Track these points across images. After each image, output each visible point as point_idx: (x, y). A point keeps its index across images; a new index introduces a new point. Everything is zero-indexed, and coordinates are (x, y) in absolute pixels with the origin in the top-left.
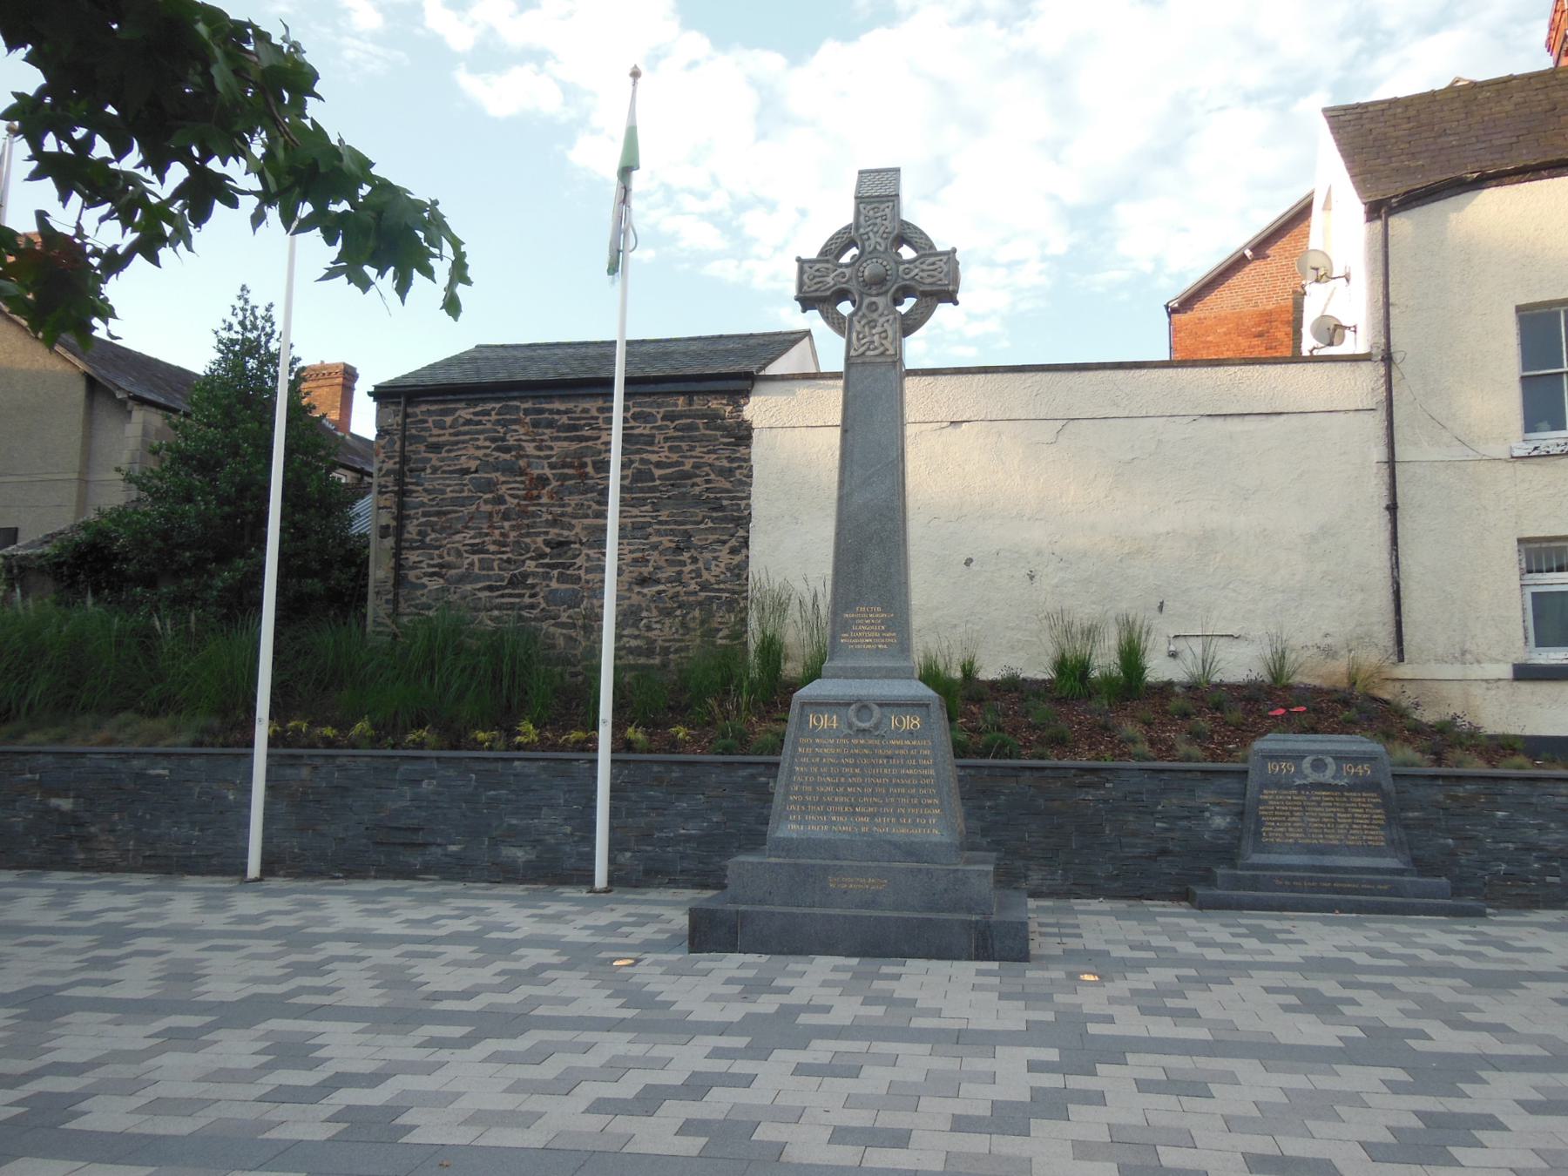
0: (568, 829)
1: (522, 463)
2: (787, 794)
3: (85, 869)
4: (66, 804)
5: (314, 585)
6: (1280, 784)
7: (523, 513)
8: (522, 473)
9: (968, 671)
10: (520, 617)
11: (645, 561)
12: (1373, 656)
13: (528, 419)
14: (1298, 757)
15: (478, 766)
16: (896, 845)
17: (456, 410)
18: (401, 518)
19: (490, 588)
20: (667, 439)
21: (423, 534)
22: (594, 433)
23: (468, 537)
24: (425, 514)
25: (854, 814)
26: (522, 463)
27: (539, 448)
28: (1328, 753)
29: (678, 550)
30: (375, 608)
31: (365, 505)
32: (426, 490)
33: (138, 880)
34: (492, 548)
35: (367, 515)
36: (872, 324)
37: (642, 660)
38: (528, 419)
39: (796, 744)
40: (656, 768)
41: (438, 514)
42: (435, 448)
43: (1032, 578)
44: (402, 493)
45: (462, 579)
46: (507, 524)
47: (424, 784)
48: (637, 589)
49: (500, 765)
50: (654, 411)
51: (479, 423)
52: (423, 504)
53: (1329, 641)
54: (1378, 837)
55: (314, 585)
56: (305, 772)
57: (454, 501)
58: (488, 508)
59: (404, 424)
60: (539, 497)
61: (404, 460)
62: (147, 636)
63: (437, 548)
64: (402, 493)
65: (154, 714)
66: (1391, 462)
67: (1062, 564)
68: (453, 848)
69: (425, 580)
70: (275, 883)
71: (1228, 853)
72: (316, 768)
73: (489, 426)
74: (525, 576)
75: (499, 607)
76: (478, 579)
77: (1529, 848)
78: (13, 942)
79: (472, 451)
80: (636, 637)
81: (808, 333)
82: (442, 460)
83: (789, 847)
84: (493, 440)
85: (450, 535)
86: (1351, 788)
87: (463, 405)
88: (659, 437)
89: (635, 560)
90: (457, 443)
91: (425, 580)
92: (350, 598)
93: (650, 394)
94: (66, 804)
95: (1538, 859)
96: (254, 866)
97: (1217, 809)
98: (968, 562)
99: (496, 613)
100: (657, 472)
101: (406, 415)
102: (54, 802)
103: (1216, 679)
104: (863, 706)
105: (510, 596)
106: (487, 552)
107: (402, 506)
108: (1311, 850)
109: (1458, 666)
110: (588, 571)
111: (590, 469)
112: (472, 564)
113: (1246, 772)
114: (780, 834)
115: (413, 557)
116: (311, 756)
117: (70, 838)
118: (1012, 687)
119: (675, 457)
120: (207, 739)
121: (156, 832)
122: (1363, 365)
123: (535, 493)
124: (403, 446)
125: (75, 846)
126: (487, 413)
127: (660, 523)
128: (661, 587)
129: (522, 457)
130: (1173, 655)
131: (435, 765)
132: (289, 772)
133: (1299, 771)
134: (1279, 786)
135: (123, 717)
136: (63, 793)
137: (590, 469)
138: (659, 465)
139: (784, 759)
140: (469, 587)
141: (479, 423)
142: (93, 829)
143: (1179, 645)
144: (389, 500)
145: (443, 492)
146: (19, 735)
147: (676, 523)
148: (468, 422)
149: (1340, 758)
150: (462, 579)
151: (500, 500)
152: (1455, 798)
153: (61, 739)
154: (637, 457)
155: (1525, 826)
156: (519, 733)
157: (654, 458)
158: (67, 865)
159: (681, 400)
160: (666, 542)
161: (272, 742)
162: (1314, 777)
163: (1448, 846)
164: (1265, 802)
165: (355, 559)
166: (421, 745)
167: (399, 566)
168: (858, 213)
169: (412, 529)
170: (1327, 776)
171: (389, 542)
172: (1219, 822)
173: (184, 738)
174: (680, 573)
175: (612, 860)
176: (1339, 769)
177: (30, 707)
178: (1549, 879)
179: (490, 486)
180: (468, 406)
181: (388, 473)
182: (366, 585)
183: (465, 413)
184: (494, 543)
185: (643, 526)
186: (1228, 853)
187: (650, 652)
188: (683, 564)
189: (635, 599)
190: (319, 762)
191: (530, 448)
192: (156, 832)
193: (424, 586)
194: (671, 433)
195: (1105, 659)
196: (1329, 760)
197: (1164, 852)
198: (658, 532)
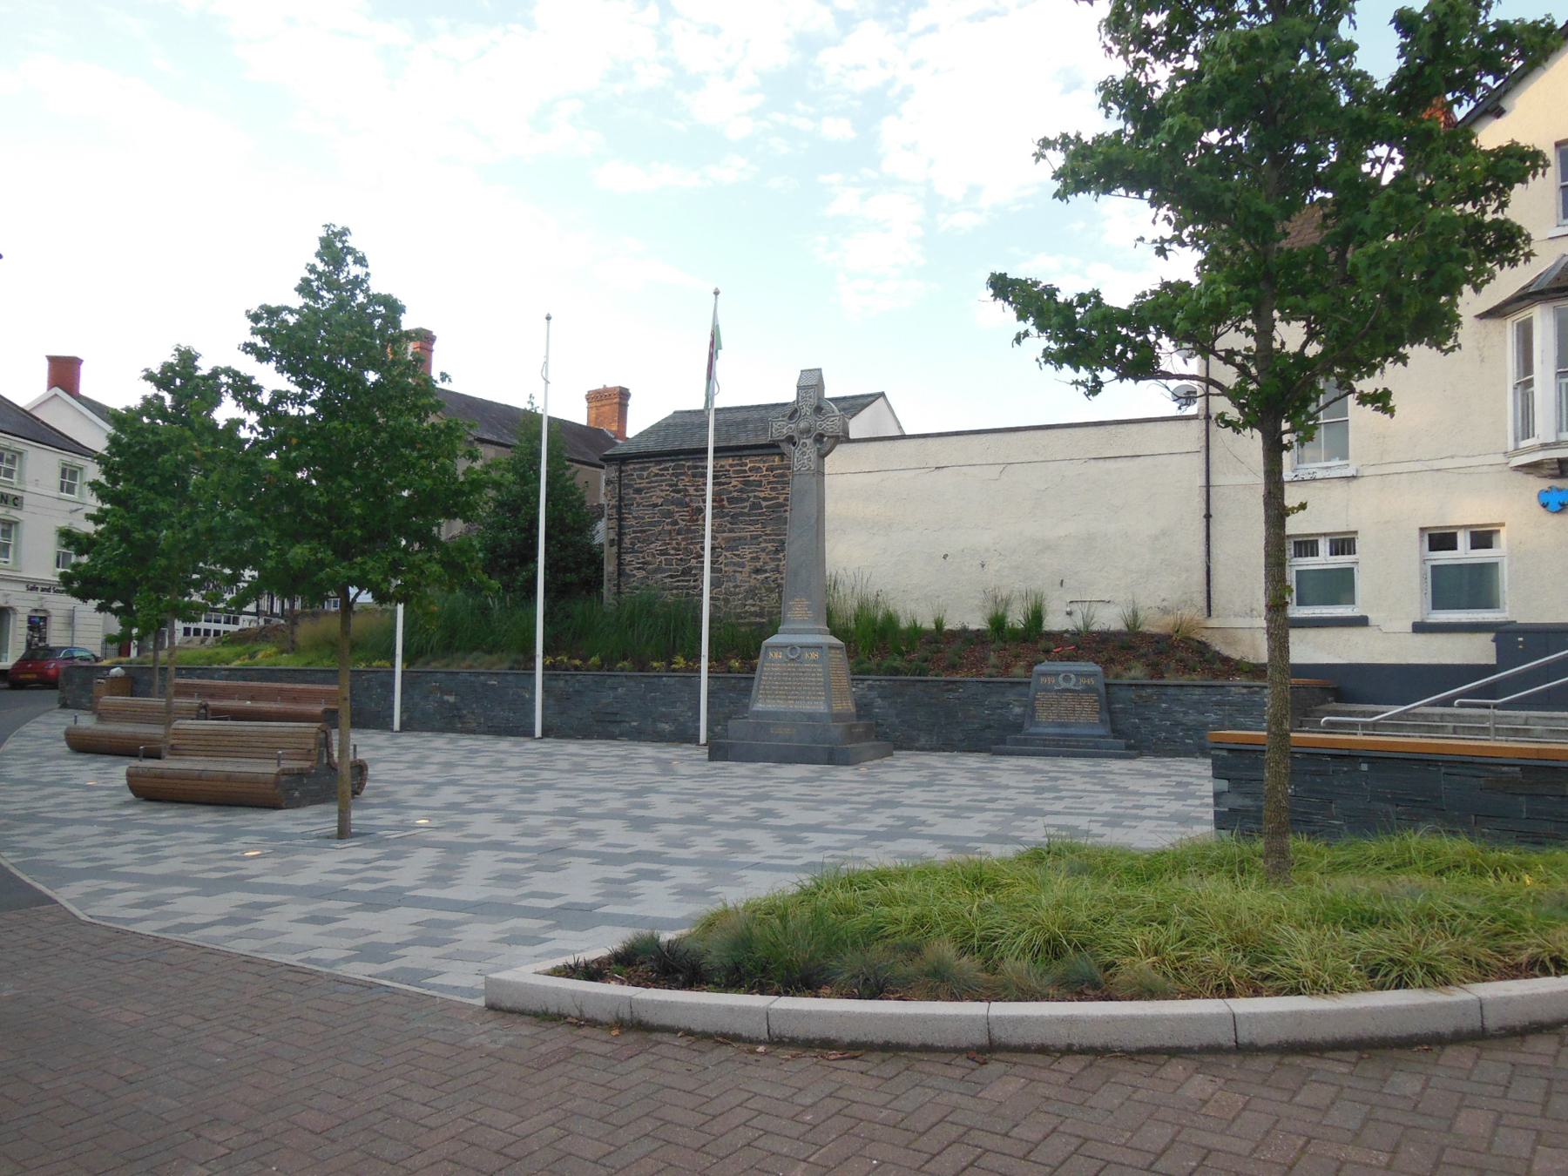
0: (690, 714)
1: (687, 499)
2: (759, 689)
3: (461, 732)
4: (451, 699)
5: (571, 577)
6: (1046, 690)
7: (689, 531)
8: (688, 505)
9: (939, 624)
10: (688, 594)
11: (757, 559)
12: (1192, 612)
13: (690, 473)
14: (1057, 674)
15: (645, 680)
16: (804, 714)
17: (649, 467)
18: (620, 534)
19: (671, 576)
20: (769, 483)
21: (633, 544)
22: (728, 480)
23: (657, 545)
24: (634, 532)
25: (787, 700)
26: (687, 499)
27: (696, 490)
28: (1071, 672)
29: (777, 551)
30: (607, 589)
31: (601, 525)
32: (634, 517)
33: (486, 737)
34: (672, 552)
35: (602, 532)
36: (804, 454)
37: (758, 620)
38: (690, 473)
39: (762, 667)
40: (733, 681)
41: (641, 532)
42: (638, 491)
43: (983, 566)
44: (621, 519)
45: (656, 571)
46: (680, 537)
47: (620, 690)
48: (754, 576)
49: (656, 680)
50: (761, 465)
51: (663, 475)
52: (632, 526)
53: (1165, 603)
54: (1095, 719)
55: (571, 577)
56: (561, 683)
57: (650, 524)
58: (669, 527)
59: (620, 477)
60: (697, 520)
61: (621, 499)
62: (486, 609)
63: (641, 552)
64: (621, 519)
65: (490, 652)
66: (1208, 486)
67: (1000, 557)
68: (635, 724)
69: (635, 572)
70: (547, 740)
71: (1018, 727)
72: (567, 681)
73: (668, 477)
74: (691, 569)
75: (677, 588)
76: (664, 571)
77: (1177, 724)
78: (373, 938)
79: (659, 493)
80: (753, 605)
81: (882, 395)
82: (642, 498)
83: (758, 714)
84: (671, 486)
85: (648, 545)
86: (1083, 691)
87: (652, 464)
88: (764, 482)
89: (752, 558)
90: (650, 488)
91: (635, 572)
92: (592, 584)
93: (758, 455)
94: (451, 699)
95: (1182, 730)
96: (538, 732)
97: (1016, 703)
98: (945, 557)
99: (675, 592)
100: (764, 504)
101: (621, 472)
102: (446, 698)
103: (1095, 628)
104: (793, 648)
105: (683, 581)
106: (669, 554)
107: (620, 527)
108: (1061, 725)
109: (1248, 619)
110: (726, 565)
111: (725, 503)
112: (661, 562)
113: (1030, 683)
114: (755, 709)
115: (628, 558)
116: (565, 675)
117: (454, 716)
118: (963, 635)
119: (774, 494)
120: (516, 666)
121: (493, 714)
122: (1193, 422)
123: (695, 517)
124: (620, 491)
125: (457, 720)
126: (667, 469)
127: (766, 535)
128: (768, 575)
129: (686, 496)
130: (1069, 614)
131: (624, 680)
132: (554, 683)
133: (1057, 683)
134: (1045, 690)
135: (475, 654)
136: (450, 693)
137: (725, 503)
138: (765, 499)
139: (757, 675)
140: (659, 576)
141: (663, 475)
142: (465, 712)
143: (1074, 607)
144: (614, 523)
145: (644, 518)
146: (427, 663)
147: (776, 535)
148: (656, 475)
149: (1078, 675)
150: (656, 571)
151: (675, 523)
152: (1141, 697)
153: (447, 666)
154: (751, 495)
155: (1176, 711)
156: (675, 663)
157: (762, 495)
158: (454, 730)
159: (777, 458)
160: (770, 546)
161: (545, 668)
162: (1064, 685)
163: (1135, 723)
164: (1038, 699)
165: (595, 560)
166: (622, 670)
167: (620, 564)
168: (798, 394)
169: (627, 541)
170: (1071, 686)
171: (615, 549)
172: (1017, 710)
173: (506, 665)
174: (778, 565)
175: (709, 729)
176: (1078, 681)
177: (432, 648)
178: (1187, 741)
179: (669, 514)
180: (656, 465)
181: (613, 507)
182: (602, 576)
183: (655, 470)
184: (673, 549)
185: (757, 537)
186: (1018, 727)
187: (761, 615)
188: (780, 560)
189: (753, 582)
190: (568, 678)
191: (691, 490)
192: (493, 714)
193: (634, 576)
194: (771, 479)
195: (1016, 618)
196: (1072, 676)
197: (990, 727)
198: (765, 541)
